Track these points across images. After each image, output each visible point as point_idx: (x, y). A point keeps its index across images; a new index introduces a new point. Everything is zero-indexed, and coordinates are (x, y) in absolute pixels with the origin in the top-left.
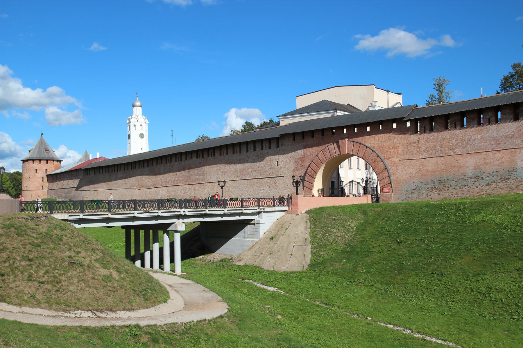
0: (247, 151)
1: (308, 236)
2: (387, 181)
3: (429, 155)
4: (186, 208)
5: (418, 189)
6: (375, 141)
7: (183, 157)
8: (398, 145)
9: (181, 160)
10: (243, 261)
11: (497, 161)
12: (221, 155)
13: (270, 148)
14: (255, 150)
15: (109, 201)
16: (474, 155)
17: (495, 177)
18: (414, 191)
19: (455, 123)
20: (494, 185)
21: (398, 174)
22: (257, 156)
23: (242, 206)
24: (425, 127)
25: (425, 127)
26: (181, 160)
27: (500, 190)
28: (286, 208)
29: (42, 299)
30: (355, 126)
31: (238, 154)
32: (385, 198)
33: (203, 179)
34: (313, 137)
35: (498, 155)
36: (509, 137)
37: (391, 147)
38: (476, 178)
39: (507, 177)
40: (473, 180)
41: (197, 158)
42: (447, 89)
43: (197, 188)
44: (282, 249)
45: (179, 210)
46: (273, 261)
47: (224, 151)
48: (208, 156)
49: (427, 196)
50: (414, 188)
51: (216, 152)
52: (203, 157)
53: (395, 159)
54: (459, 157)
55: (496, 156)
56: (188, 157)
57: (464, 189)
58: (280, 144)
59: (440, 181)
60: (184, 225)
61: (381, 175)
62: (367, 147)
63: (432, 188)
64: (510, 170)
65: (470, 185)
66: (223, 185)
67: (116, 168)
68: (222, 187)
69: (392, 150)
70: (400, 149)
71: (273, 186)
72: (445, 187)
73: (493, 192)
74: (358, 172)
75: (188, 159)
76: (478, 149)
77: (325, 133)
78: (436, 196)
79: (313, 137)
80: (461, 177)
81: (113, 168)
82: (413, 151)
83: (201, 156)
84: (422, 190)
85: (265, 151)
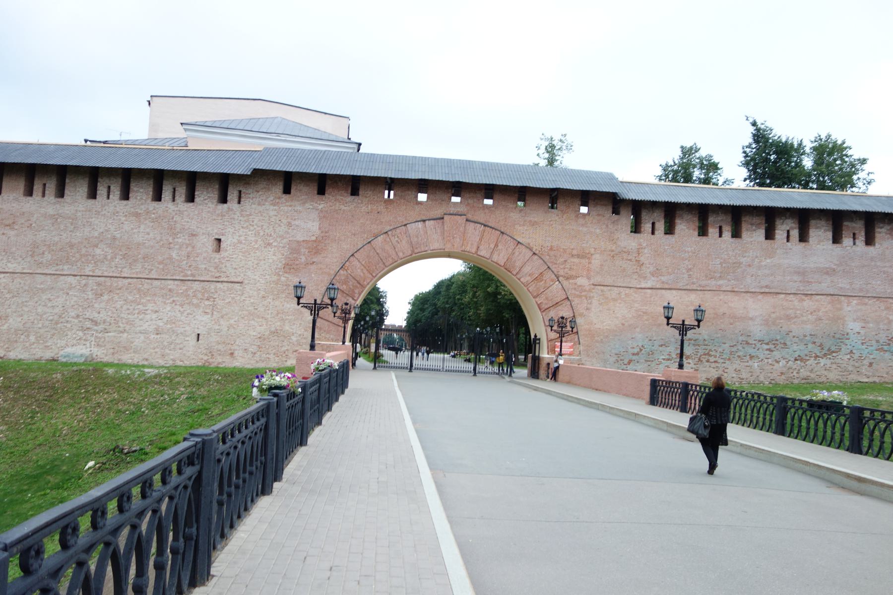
0: (44, 195)
3: (663, 283)
8: (592, 251)
11: (807, 317)
16: (760, 297)
17: (810, 346)
18: (634, 357)
19: (720, 228)
20: (812, 361)
22: (137, 215)
24: (653, 224)
25: (653, 224)
27: (826, 373)
29: (547, 298)
34: (355, 192)
35: (808, 303)
36: (827, 273)
37: (575, 252)
38: (774, 343)
39: (833, 348)
40: (768, 347)
50: (635, 351)
53: (582, 281)
54: (729, 297)
55: (805, 303)
57: (750, 363)
58: (232, 195)
64: (837, 336)
65: (762, 356)
68: (683, 329)
69: (576, 260)
70: (596, 260)
71: (197, 306)
72: (708, 354)
73: (812, 376)
76: (766, 287)
77: (328, 190)
79: (287, 191)
80: (741, 338)
82: (624, 270)
85: (171, 205)
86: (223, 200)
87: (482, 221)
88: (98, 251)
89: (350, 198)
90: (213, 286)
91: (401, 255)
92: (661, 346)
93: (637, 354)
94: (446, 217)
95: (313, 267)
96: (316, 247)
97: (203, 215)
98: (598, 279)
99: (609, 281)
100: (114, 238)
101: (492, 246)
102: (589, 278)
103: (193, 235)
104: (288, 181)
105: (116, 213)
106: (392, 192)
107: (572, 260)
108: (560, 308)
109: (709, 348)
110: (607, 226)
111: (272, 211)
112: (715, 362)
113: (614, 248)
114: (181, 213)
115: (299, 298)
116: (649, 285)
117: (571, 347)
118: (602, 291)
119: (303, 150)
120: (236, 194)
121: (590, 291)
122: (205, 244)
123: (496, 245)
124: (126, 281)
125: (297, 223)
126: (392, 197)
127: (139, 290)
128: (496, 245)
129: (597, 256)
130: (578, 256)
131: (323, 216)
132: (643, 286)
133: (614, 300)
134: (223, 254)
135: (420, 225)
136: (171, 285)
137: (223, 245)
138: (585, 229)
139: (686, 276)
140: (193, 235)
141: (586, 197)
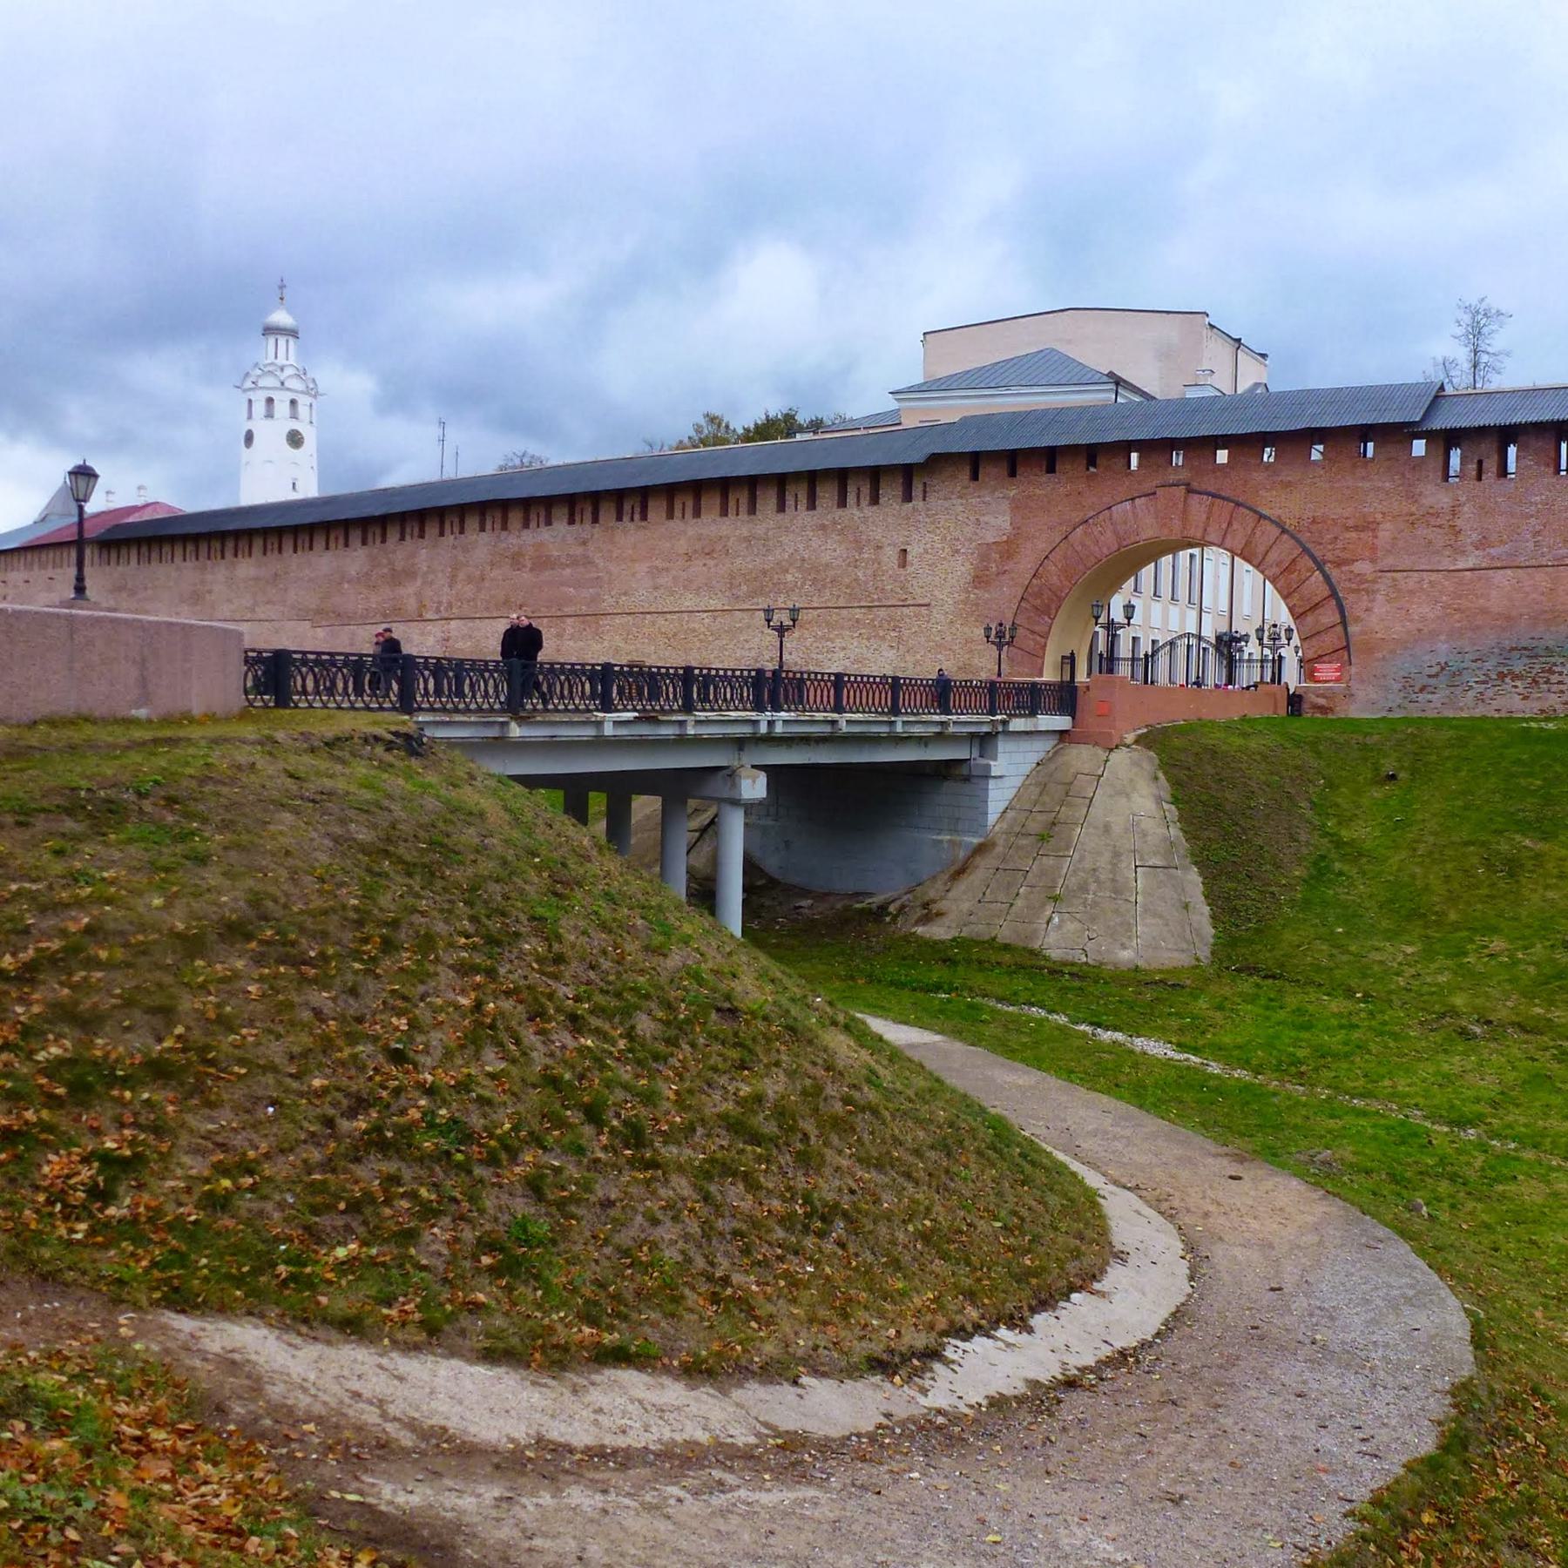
0: (781, 508)
1: (1175, 832)
2: (1331, 640)
4: (777, 708)
5: (1449, 673)
6: (1300, 495)
7: (515, 517)
8: (1379, 517)
9: (504, 527)
10: (946, 920)
12: (670, 516)
13: (875, 500)
14: (812, 505)
15: (893, 678)
18: (1432, 681)
21: (1374, 619)
22: (823, 527)
23: (838, 709)
24: (1480, 463)
25: (1480, 463)
26: (504, 527)
28: (1062, 722)
30: (1170, 444)
31: (743, 516)
32: (1322, 701)
33: (595, 599)
34: (1051, 469)
37: (1350, 523)
41: (571, 522)
42: (1497, 341)
43: (569, 630)
44: (1097, 881)
45: (753, 715)
46: (1071, 926)
47: (452, 521)
48: (619, 518)
49: (1481, 698)
51: (651, 504)
52: (595, 520)
53: (1359, 567)
56: (533, 516)
58: (917, 490)
59: (1530, 653)
60: (762, 779)
61: (1310, 619)
62: (1262, 517)
63: (1502, 676)
66: (788, 622)
67: (230, 545)
68: (781, 630)
69: (1354, 535)
70: (1386, 533)
71: (883, 638)
72: (1551, 671)
74: (1174, 611)
75: (533, 524)
77: (1020, 470)
78: (1516, 703)
79: (975, 477)
81: (217, 545)
83: (588, 515)
84: (1466, 677)
85: (855, 511)
86: (908, 498)
87: (1211, 489)
88: (789, 577)
89: (1045, 478)
90: (899, 611)
91: (1105, 551)
92: (1475, 661)
93: (1436, 676)
94: (1160, 492)
95: (1006, 576)
96: (1008, 549)
97: (882, 522)
98: (1389, 561)
99: (1406, 562)
100: (803, 560)
101: (1224, 526)
102: (1373, 561)
103: (879, 547)
104: (975, 462)
105: (803, 528)
106: (1370, 445)
107: (1347, 535)
108: (1321, 611)
109: (1553, 660)
110: (1403, 475)
111: (958, 505)
112: (1560, 683)
113: (1414, 509)
114: (865, 520)
115: (769, 621)
116: (1470, 565)
117: (1337, 670)
118: (1394, 580)
119: (1082, 410)
120: (920, 487)
121: (1374, 582)
122: (890, 555)
123: (1230, 524)
124: (816, 613)
125: (986, 519)
126: (1370, 453)
127: (828, 624)
128: (1230, 524)
129: (1388, 525)
130: (1356, 528)
131: (1016, 506)
132: (1460, 566)
133: (1411, 592)
134: (910, 569)
135: (1128, 505)
136: (858, 613)
137: (909, 558)
138: (1367, 485)
139: (1531, 545)
140: (879, 547)
141: (937, 463)
